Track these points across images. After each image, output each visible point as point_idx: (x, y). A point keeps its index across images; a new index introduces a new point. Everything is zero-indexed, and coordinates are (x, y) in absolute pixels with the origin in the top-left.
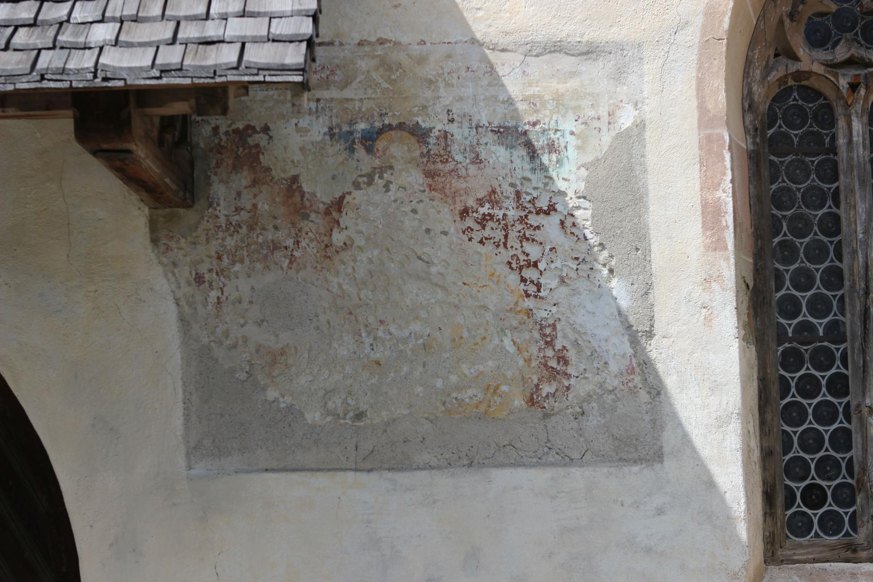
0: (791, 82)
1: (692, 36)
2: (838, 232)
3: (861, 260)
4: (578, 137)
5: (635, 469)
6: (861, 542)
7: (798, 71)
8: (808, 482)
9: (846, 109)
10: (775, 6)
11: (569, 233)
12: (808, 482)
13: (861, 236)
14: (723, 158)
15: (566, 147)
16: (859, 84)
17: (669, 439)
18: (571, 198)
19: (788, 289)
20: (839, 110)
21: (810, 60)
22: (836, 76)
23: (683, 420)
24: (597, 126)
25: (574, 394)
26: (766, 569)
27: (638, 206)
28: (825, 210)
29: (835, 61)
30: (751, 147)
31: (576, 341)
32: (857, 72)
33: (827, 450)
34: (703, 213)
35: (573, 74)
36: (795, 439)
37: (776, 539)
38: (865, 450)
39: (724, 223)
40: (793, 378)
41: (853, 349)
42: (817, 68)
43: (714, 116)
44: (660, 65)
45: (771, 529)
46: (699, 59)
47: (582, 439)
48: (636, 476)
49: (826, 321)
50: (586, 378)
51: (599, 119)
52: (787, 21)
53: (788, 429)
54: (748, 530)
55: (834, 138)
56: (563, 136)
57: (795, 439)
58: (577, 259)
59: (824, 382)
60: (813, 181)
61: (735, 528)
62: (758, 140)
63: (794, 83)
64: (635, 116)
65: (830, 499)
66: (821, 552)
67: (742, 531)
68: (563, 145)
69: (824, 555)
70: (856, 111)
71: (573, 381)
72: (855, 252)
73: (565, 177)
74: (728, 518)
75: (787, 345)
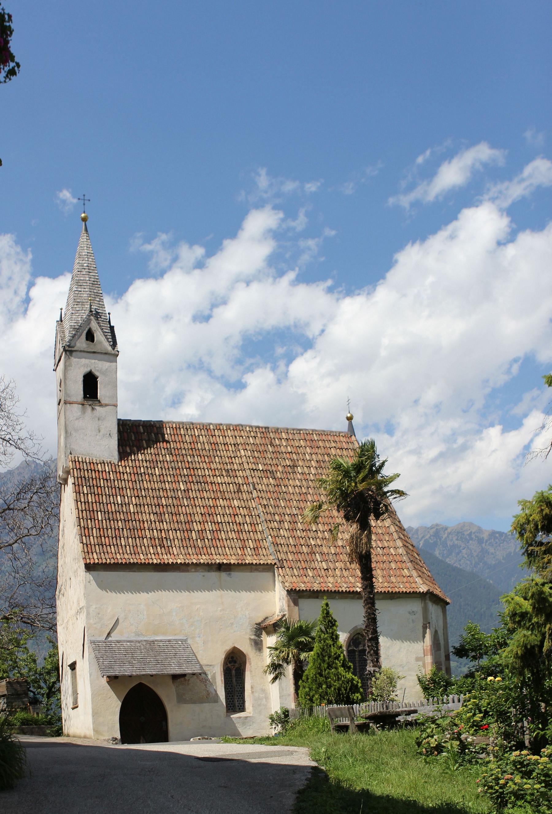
21: (229, 665)
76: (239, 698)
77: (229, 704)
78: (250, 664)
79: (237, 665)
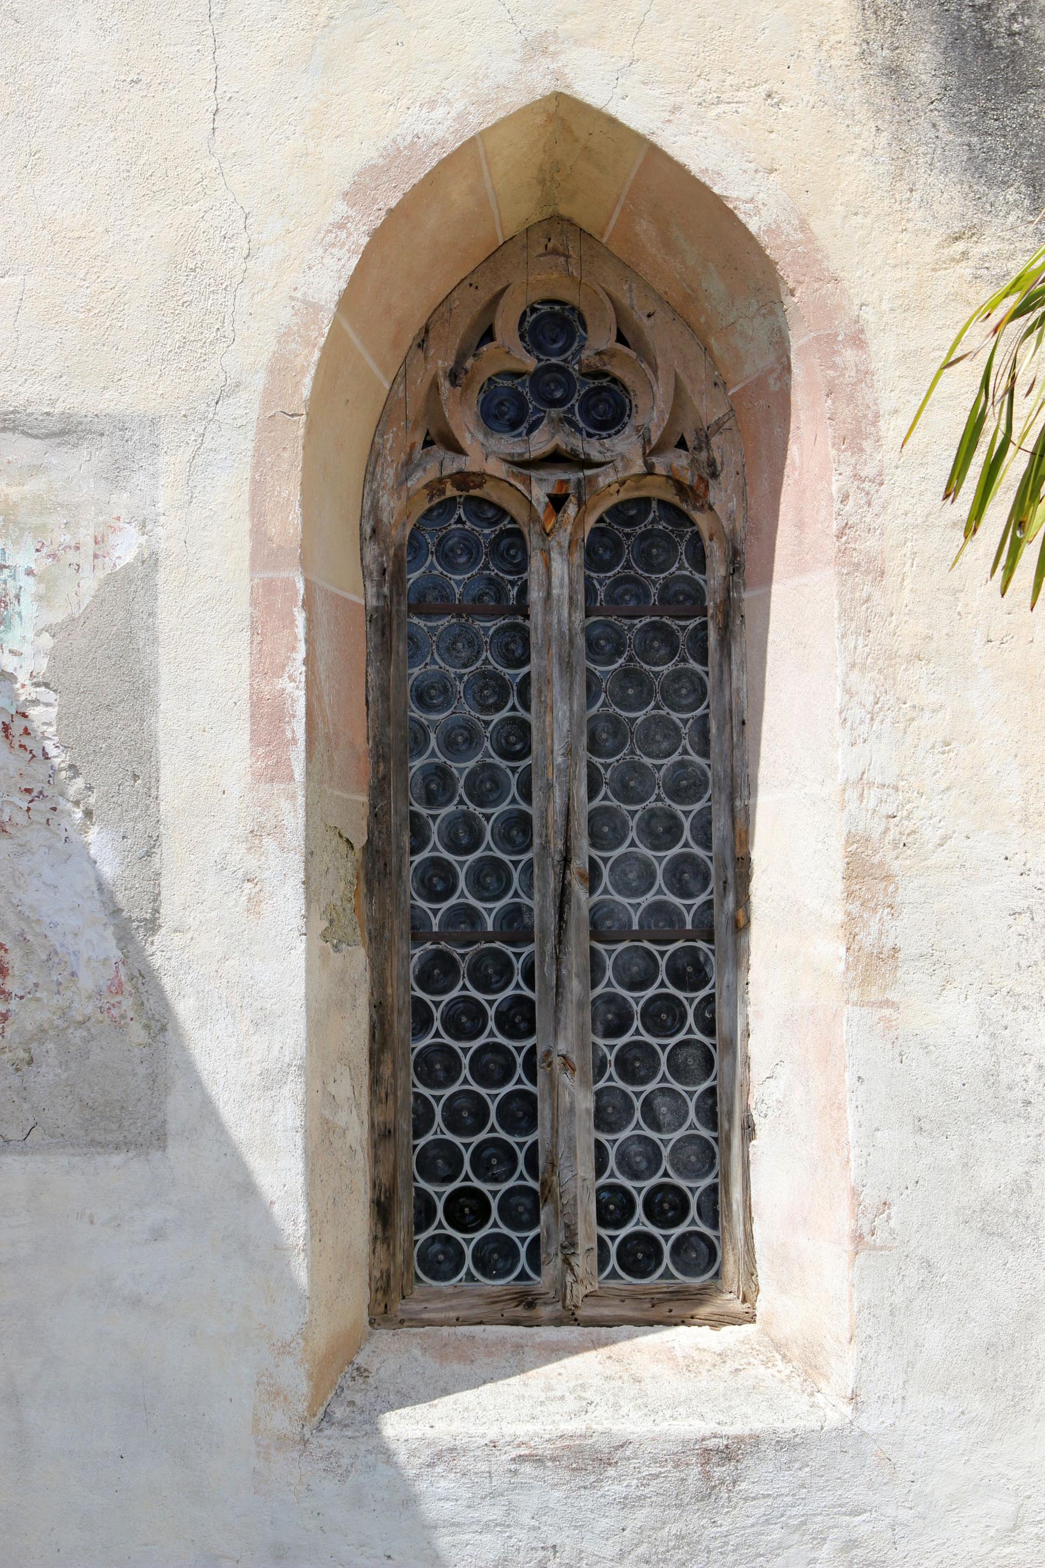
0: (451, 491)
1: (246, 407)
2: (526, 752)
3: (558, 801)
4: (40, 579)
5: (117, 1159)
6: (543, 1290)
7: (460, 473)
8: (457, 1184)
9: (544, 540)
10: (426, 358)
11: (17, 746)
12: (457, 1184)
13: (559, 760)
14: (293, 621)
15: (18, 597)
16: (566, 496)
17: (177, 1107)
18: (23, 686)
19: (436, 848)
20: (533, 541)
21: (484, 452)
22: (527, 481)
23: (205, 1076)
24: (74, 561)
25: (15, 1026)
26: (371, 1334)
27: (140, 702)
28: (505, 713)
29: (527, 456)
30: (373, 602)
31: (22, 934)
32: (565, 476)
33: (493, 1130)
34: (252, 716)
35: (36, 469)
36: (438, 1110)
37: (392, 1284)
38: (555, 1131)
39: (289, 735)
40: (437, 1004)
41: (543, 954)
42: (495, 468)
43: (280, 547)
44: (187, 456)
45: (384, 1266)
46: (257, 449)
47: (26, 1106)
48: (118, 1172)
49: (498, 905)
50: (38, 1000)
51: (77, 548)
52: (445, 385)
53: (426, 1092)
54: (312, 1269)
55: (524, 590)
56: (13, 577)
57: (438, 1110)
58: (28, 791)
59: (491, 1012)
60: (486, 661)
61: (288, 1264)
62: (386, 590)
63: (456, 493)
64: (140, 546)
65: (495, 1214)
66: (473, 1306)
67: (301, 1271)
68: (12, 592)
69: (476, 1311)
70: (559, 543)
71: (13, 1004)
72: (550, 786)
73: (15, 648)
74: (276, 1248)
75: (429, 946)
76: (635, 1064)
77: (439, 1162)
78: (856, 436)
79: (621, 459)
